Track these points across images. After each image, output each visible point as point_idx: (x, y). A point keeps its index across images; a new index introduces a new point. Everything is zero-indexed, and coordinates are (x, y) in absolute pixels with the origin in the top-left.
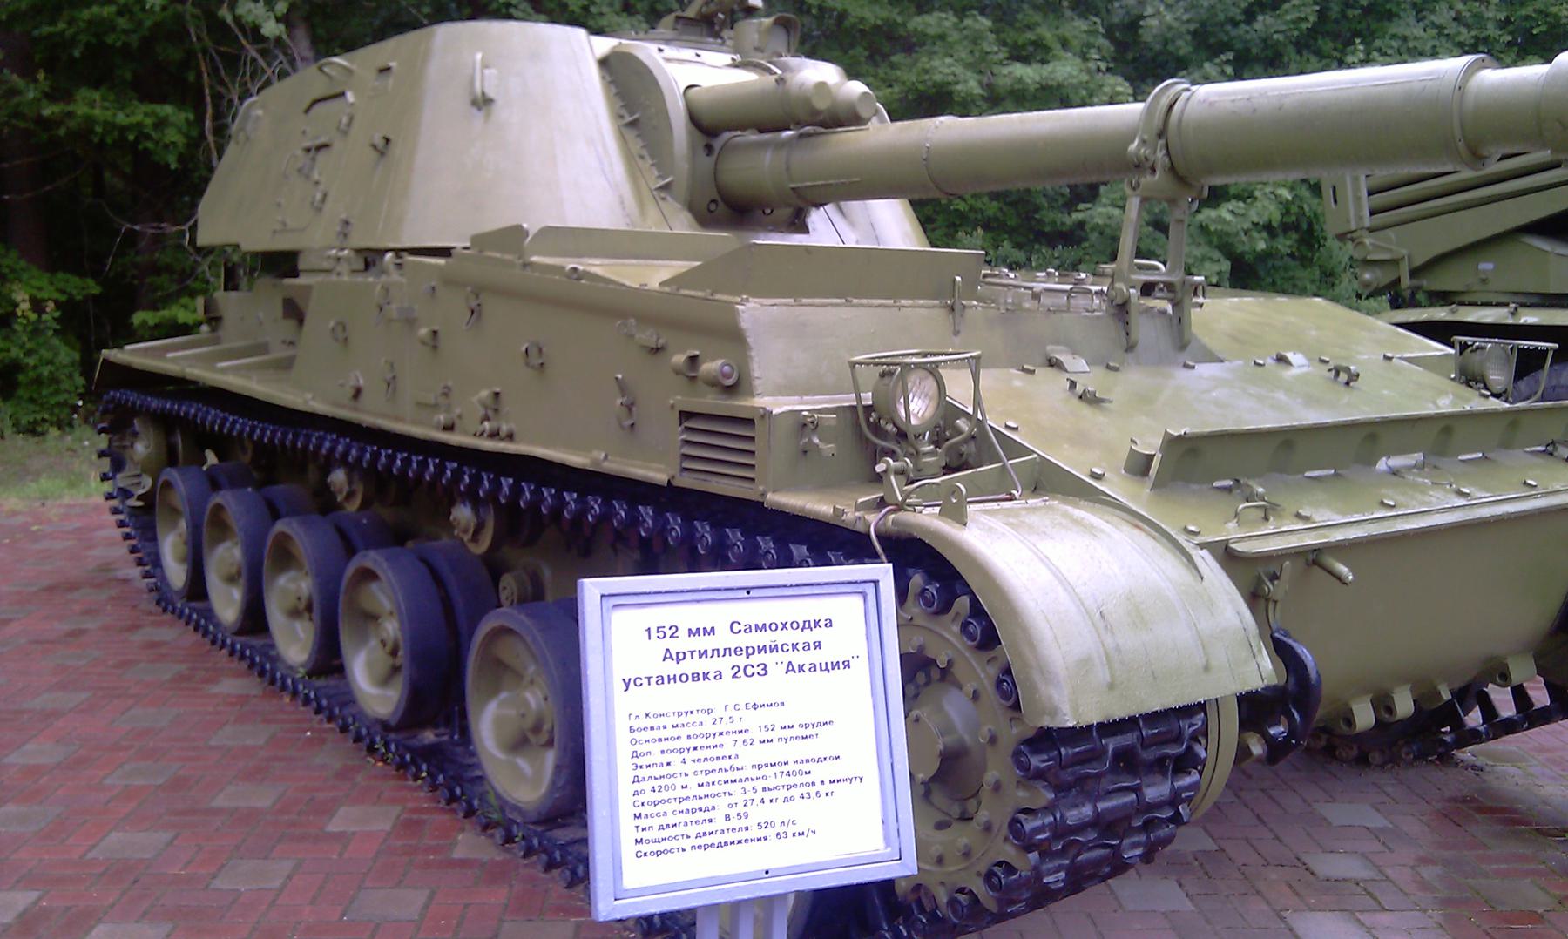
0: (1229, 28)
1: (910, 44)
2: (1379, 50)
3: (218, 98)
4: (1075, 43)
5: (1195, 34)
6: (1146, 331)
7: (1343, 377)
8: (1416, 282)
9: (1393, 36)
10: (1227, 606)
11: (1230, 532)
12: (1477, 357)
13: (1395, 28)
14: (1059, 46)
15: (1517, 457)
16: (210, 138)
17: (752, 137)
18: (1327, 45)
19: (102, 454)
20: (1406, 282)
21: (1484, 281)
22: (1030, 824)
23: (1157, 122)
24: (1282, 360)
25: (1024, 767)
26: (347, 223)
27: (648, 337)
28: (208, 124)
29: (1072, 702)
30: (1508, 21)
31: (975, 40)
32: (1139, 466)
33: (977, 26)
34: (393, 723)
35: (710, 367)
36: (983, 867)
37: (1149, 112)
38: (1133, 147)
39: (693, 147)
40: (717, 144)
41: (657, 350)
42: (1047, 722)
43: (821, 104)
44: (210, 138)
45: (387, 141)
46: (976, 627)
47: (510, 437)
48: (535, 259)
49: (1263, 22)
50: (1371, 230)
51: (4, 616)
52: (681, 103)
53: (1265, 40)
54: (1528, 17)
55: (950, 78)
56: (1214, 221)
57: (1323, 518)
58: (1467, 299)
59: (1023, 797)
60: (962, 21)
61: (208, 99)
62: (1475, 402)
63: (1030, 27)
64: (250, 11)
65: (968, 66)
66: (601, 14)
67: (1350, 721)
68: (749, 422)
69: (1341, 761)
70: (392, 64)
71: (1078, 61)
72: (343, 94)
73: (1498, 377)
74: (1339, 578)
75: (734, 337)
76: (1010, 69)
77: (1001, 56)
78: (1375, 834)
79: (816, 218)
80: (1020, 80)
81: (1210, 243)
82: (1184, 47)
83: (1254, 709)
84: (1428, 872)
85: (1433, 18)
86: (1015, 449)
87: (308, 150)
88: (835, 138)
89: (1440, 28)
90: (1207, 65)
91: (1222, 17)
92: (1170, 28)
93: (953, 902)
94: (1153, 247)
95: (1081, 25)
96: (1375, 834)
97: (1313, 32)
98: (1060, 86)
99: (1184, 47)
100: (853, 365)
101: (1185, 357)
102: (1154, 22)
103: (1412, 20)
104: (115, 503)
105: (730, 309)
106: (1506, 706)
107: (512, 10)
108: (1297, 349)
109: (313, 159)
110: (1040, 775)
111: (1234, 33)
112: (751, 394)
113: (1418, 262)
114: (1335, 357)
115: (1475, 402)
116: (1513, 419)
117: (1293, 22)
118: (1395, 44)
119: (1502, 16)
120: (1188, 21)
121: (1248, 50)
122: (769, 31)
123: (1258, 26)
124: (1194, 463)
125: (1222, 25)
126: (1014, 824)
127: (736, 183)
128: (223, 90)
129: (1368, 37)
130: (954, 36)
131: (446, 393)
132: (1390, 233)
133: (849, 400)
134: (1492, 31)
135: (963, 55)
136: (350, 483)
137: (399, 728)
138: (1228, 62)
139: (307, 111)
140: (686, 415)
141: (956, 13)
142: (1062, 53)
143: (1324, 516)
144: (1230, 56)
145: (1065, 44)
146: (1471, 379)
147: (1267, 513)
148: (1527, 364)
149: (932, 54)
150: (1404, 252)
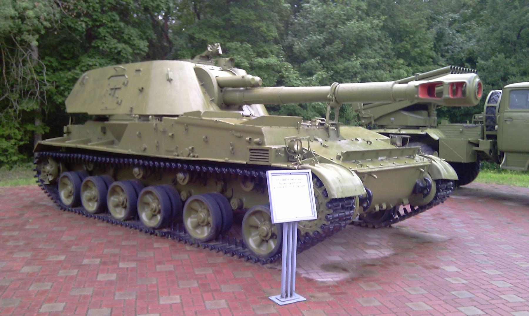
0: (318, 49)
2: (360, 57)
3: (7, 63)
4: (275, 52)
5: (308, 50)
6: (332, 133)
7: (369, 143)
8: (375, 123)
9: (364, 53)
10: (357, 180)
11: (356, 168)
12: (394, 139)
13: (364, 51)
15: (404, 158)
16: (4, 75)
17: (231, 89)
18: (345, 55)
19: (35, 170)
20: (373, 123)
21: (392, 123)
22: (329, 216)
23: (333, 91)
24: (357, 139)
25: (328, 207)
27: (238, 134)
28: (4, 71)
29: (337, 194)
30: (394, 48)
31: (246, 50)
32: (339, 158)
33: (247, 47)
34: (157, 227)
35: (257, 140)
36: (320, 226)
37: (332, 89)
38: (328, 96)
39: (218, 90)
40: (223, 90)
41: (240, 137)
42: (333, 197)
43: (253, 83)
44: (4, 75)
45: (142, 88)
46: (318, 184)
47: (197, 157)
48: (203, 118)
49: (328, 48)
50: (363, 109)
51: (1, 218)
52: (216, 81)
53: (328, 53)
54: (399, 48)
55: (240, 62)
56: (317, 105)
57: (370, 167)
58: (388, 127)
59: (327, 212)
60: (242, 45)
61: (4, 63)
62: (394, 147)
63: (262, 47)
64: (28, 38)
65: (245, 58)
66: (134, 40)
67: (375, 209)
68: (268, 150)
69: (369, 228)
70: (141, 69)
71: (276, 58)
72: (124, 75)
73: (399, 143)
74: (374, 177)
75: (260, 134)
76: (257, 59)
77: (254, 55)
78: (378, 239)
79: (245, 107)
80: (260, 63)
81: (316, 111)
82: (306, 54)
83: (362, 200)
84: (389, 244)
85: (374, 48)
86: (316, 155)
87: (112, 89)
88: (255, 90)
89: (376, 50)
90: (313, 60)
91: (316, 46)
92: (302, 48)
93: (314, 233)
94: (300, 112)
95: (276, 47)
96: (378, 239)
97: (341, 52)
98: (272, 65)
99: (306, 54)
100: (285, 139)
101: (339, 139)
102: (297, 47)
103: (368, 48)
104: (40, 183)
105: (261, 130)
106: (402, 212)
107: (106, 38)
108: (359, 137)
109: (115, 92)
110: (330, 208)
111: (320, 51)
112: (265, 145)
113: (376, 117)
114: (367, 139)
115: (394, 147)
116: (402, 151)
117: (336, 48)
118: (364, 55)
119: (392, 47)
120: (307, 47)
121: (324, 56)
122: (228, 61)
123: (326, 49)
124: (348, 157)
125: (316, 48)
126: (326, 217)
127: (227, 98)
128: (9, 60)
129: (356, 53)
130: (240, 49)
131: (177, 148)
132: (369, 110)
133: (285, 146)
134: (390, 51)
135: (243, 55)
136: (139, 171)
137: (158, 229)
138: (319, 59)
139: (109, 79)
140: (251, 150)
141: (241, 43)
142: (271, 55)
143: (371, 167)
144: (319, 57)
145: (272, 52)
146: (393, 143)
147: (362, 166)
148: (404, 142)
149: (233, 54)
150: (372, 115)
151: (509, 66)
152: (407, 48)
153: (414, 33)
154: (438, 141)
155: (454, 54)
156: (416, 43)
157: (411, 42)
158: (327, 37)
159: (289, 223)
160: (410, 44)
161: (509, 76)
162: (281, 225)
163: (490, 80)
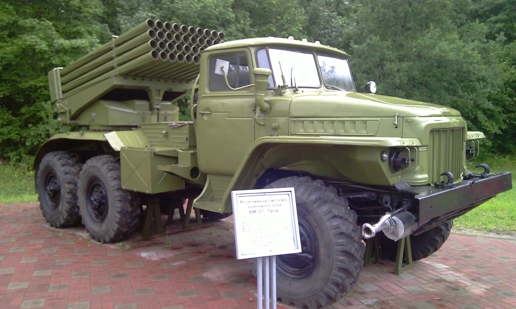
1: (23, 30)
14: (87, 33)
26: (396, 127)
54: (264, 31)
55: (33, 44)
63: (76, 26)
85: (229, 30)
130: (38, 27)
150: (67, 109)
151: (385, 50)
152: (272, 30)
153: (281, 14)
154: (119, 152)
155: (330, 39)
156: (283, 25)
157: (278, 24)
158: (163, 15)
159: (264, 258)
160: (277, 27)
161: (384, 62)
162: (252, 262)
163: (364, 67)
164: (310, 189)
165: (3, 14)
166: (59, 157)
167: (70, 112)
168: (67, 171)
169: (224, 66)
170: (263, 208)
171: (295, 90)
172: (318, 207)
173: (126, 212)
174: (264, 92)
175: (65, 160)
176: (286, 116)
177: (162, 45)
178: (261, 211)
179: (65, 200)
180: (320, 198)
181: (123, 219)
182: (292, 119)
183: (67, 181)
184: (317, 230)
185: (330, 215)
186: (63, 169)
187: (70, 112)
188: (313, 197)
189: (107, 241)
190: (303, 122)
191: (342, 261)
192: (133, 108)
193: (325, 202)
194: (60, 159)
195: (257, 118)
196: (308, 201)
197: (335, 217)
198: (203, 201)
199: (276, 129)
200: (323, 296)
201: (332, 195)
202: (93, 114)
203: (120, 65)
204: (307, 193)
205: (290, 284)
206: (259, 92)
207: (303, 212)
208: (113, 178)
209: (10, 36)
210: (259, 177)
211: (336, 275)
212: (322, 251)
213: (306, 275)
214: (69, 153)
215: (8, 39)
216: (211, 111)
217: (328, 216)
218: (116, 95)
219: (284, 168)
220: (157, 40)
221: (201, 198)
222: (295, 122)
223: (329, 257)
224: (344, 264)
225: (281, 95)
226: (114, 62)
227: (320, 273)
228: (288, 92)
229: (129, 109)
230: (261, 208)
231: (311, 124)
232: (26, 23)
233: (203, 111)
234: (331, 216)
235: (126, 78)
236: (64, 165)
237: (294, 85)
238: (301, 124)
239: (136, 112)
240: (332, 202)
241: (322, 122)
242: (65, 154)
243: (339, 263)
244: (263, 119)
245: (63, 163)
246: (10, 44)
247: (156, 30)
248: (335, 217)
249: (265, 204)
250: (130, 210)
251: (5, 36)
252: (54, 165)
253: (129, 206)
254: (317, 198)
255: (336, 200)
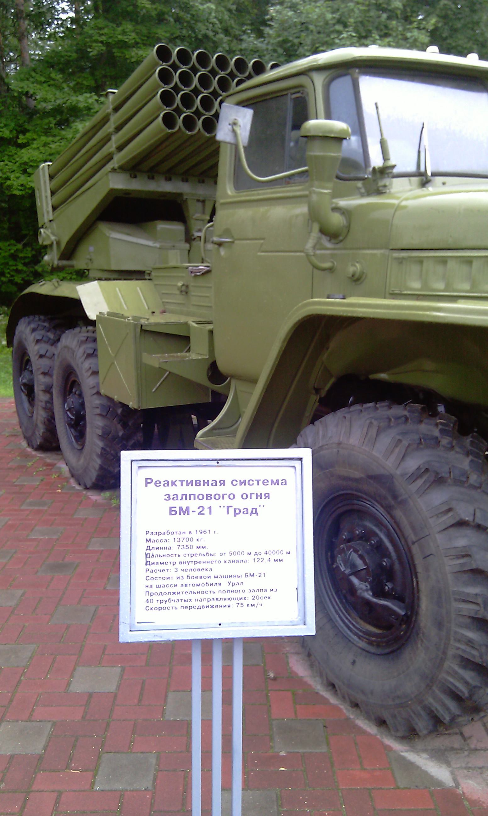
150: (53, 238)
154: (95, 321)
164: (405, 443)
165: (47, 88)
166: (33, 326)
167: (58, 243)
168: (42, 352)
169: (240, 121)
170: (212, 503)
171: (423, 179)
172: (422, 492)
173: (114, 438)
174: (330, 185)
175: (43, 332)
176: (381, 248)
177: (187, 101)
178: (206, 511)
179: (40, 404)
180: (427, 470)
181: (108, 449)
182: (396, 254)
183: (42, 370)
184: (415, 549)
185: (449, 519)
186: (37, 347)
187: (58, 243)
188: (413, 464)
189: (88, 486)
190: (420, 261)
191: (470, 642)
192: (153, 236)
193: (439, 481)
194: (34, 330)
195: (311, 252)
196: (398, 472)
197: (461, 524)
198: (219, 435)
199: (356, 280)
200: (423, 713)
201: (465, 463)
202: (92, 249)
203: (120, 148)
204: (397, 450)
205: (354, 663)
206: (316, 183)
207: (342, 516)
208: (90, 372)
209: (59, 124)
210: (323, 393)
211: (455, 674)
212: (425, 605)
213: (387, 651)
214: (51, 320)
215: (55, 131)
216: (232, 237)
217: (445, 518)
218: (123, 211)
219: (383, 376)
220: (176, 89)
221: (214, 428)
222: (401, 261)
223: (440, 625)
224: (475, 652)
225: (379, 192)
226: (112, 146)
227: (418, 657)
228: (398, 187)
229: (147, 239)
230: (206, 503)
231: (465, 268)
232: (78, 101)
233: (220, 236)
234: (453, 522)
235: (135, 177)
236: (38, 341)
237: (422, 169)
238: (415, 268)
239: (157, 245)
240: (461, 481)
241: (469, 261)
242: (44, 321)
243: (463, 647)
244: (332, 256)
245: (39, 338)
246: (58, 138)
247: (175, 67)
248: (461, 524)
249: (219, 490)
250: (121, 434)
251: (52, 125)
252: (26, 339)
253: (119, 426)
254: (419, 468)
255: (474, 478)
